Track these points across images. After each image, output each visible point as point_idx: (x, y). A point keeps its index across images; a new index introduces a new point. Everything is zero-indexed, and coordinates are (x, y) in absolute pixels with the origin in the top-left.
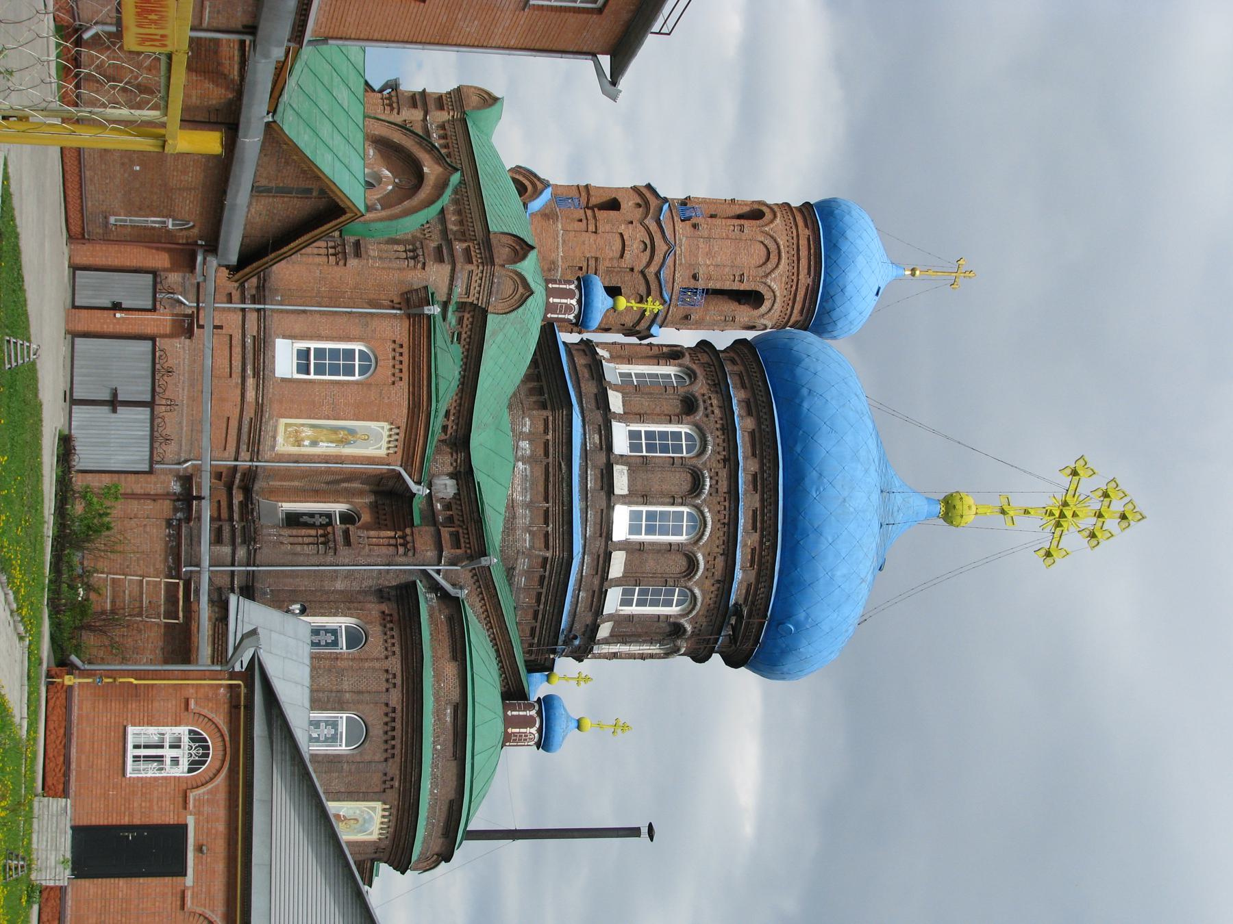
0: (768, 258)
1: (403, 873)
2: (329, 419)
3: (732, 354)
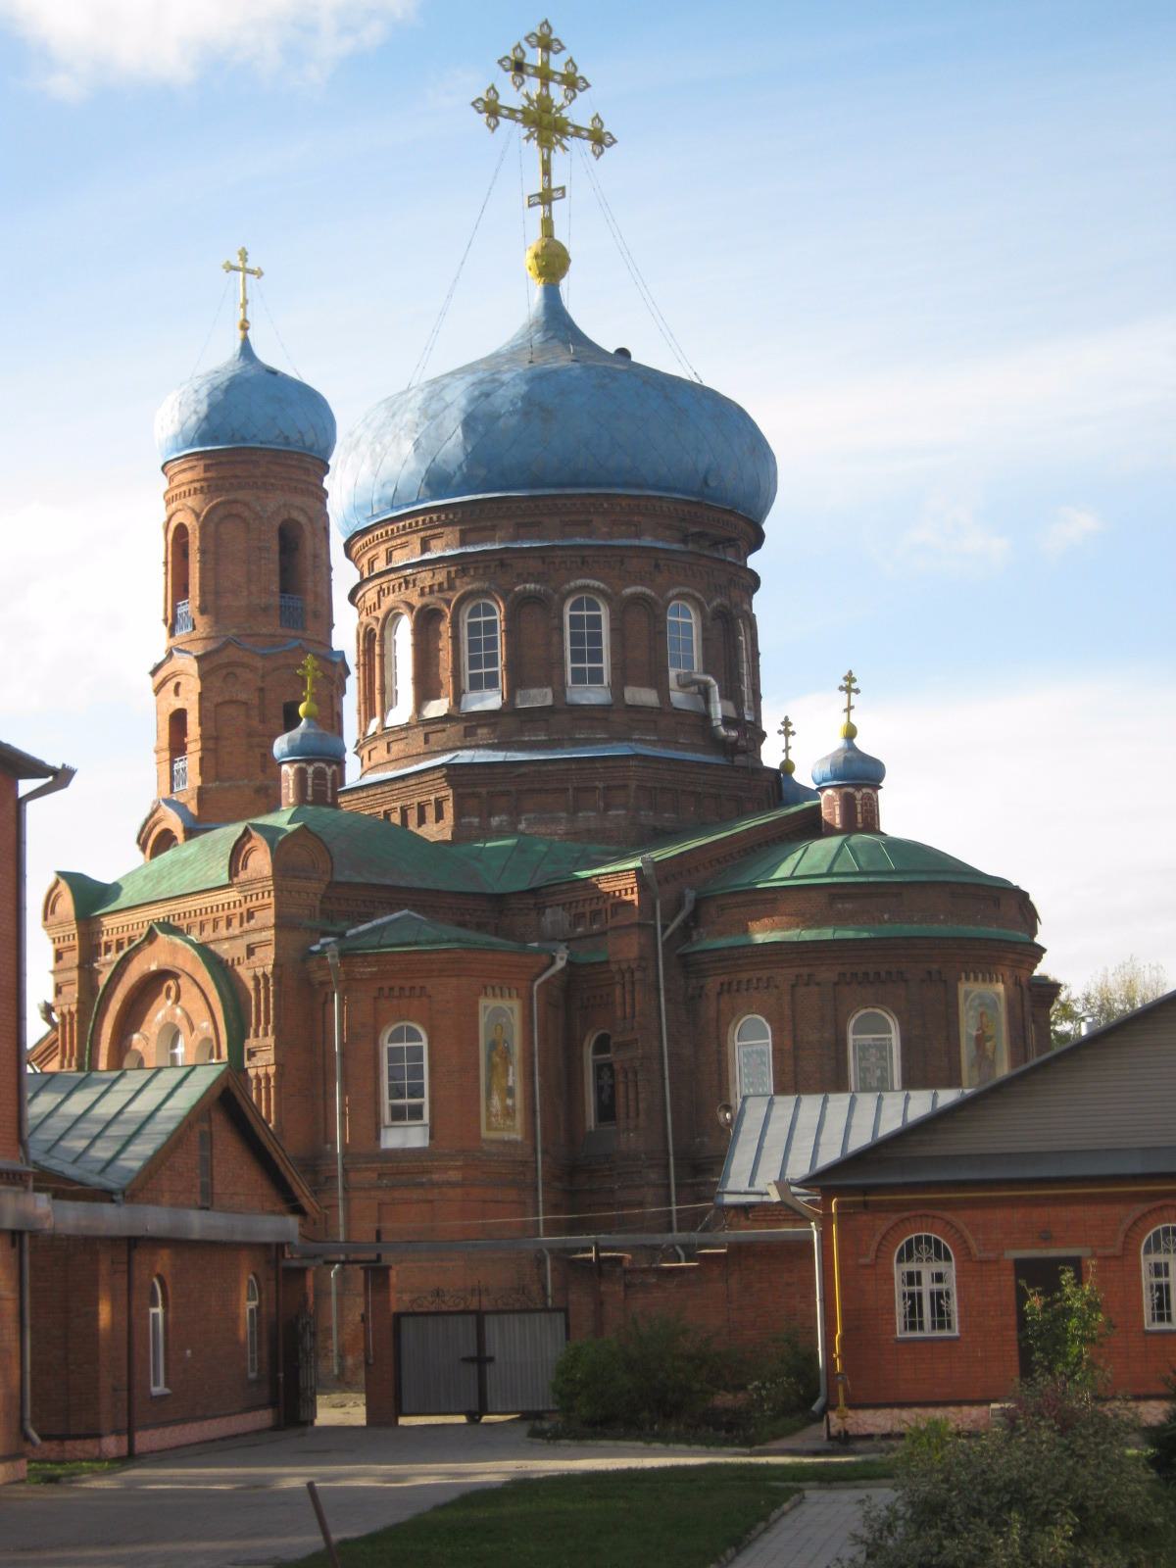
0: (238, 516)
1: (1043, 950)
2: (477, 1078)
3: (365, 561)
